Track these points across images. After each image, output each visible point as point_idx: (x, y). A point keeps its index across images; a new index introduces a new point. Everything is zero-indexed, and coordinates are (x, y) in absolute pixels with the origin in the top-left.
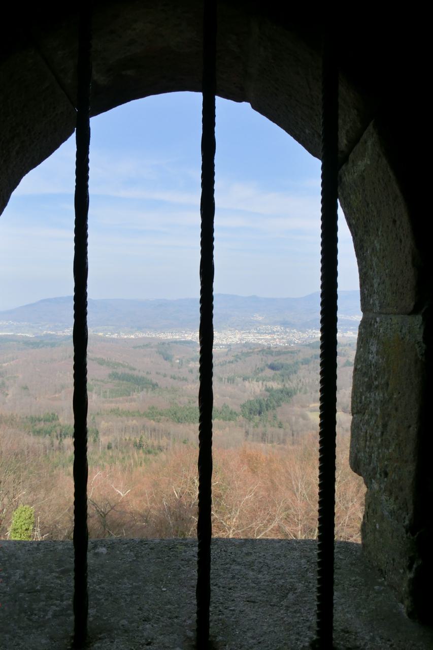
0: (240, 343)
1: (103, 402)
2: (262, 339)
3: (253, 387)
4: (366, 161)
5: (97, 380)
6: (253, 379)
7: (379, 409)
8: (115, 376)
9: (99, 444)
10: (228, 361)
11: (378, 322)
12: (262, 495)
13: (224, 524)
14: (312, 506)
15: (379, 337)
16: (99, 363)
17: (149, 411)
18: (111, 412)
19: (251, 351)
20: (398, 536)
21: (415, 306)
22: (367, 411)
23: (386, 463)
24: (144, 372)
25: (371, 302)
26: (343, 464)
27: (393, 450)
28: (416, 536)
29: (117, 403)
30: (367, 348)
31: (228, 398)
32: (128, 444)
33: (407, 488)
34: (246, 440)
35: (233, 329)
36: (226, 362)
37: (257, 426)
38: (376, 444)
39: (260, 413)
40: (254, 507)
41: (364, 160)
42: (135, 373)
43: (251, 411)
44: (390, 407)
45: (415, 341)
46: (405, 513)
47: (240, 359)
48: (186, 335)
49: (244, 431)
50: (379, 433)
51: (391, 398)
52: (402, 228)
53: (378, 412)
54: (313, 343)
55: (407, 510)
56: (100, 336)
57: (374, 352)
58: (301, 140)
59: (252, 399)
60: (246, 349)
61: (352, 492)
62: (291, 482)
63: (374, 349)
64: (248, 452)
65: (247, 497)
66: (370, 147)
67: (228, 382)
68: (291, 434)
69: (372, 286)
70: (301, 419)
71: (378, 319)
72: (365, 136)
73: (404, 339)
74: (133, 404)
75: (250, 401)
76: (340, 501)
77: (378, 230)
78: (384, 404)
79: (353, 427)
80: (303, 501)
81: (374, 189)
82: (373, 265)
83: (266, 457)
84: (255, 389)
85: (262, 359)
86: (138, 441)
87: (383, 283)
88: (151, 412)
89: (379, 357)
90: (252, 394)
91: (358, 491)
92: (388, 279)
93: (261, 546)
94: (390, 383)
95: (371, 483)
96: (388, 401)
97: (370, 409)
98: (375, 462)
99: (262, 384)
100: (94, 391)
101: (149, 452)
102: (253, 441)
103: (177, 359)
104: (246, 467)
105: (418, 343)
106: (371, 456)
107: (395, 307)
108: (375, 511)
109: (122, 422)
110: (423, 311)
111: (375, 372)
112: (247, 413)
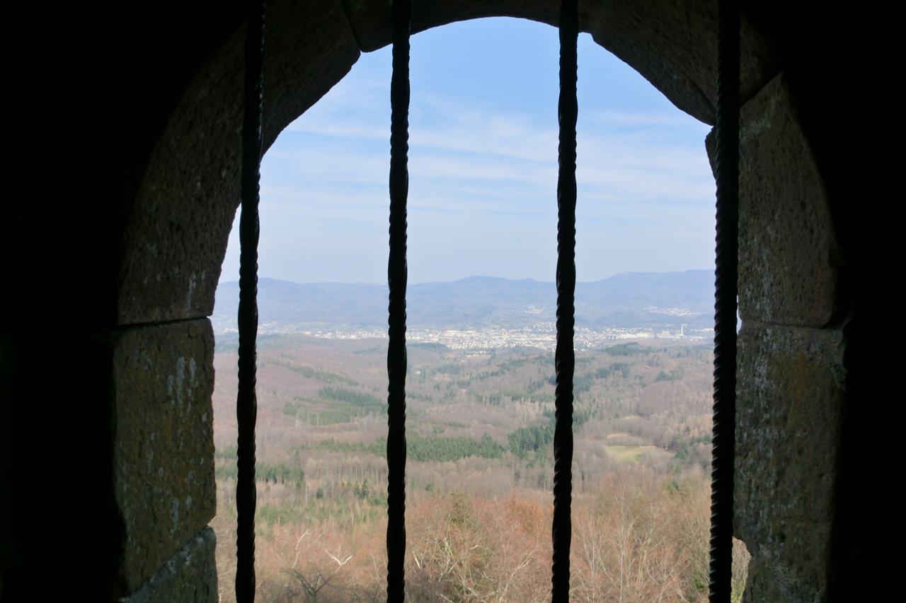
0: (509, 347)
2: (539, 341)
4: (764, 121)
5: (303, 399)
6: (526, 398)
7: (772, 452)
8: (327, 393)
10: (490, 373)
11: (770, 335)
12: (540, 564)
14: (611, 579)
15: (770, 356)
16: (305, 375)
17: (376, 443)
18: (322, 444)
19: (524, 358)
22: (750, 453)
23: (783, 522)
25: (758, 307)
26: (656, 521)
27: (795, 506)
31: (490, 425)
32: (346, 492)
33: (817, 557)
34: (515, 485)
36: (488, 373)
37: (531, 465)
38: (766, 498)
39: (536, 447)
40: (530, 580)
41: (761, 121)
42: (358, 389)
44: (789, 449)
47: (508, 370)
48: (430, 335)
49: (513, 473)
50: (772, 483)
51: (791, 437)
53: (771, 454)
54: (613, 347)
55: (817, 584)
56: (307, 336)
57: (762, 374)
59: (525, 426)
60: (516, 356)
62: (582, 546)
63: (763, 370)
64: (518, 502)
65: (519, 567)
66: (773, 107)
67: (491, 402)
68: (581, 478)
69: (759, 285)
70: (594, 457)
71: (769, 331)
72: (766, 90)
73: (814, 360)
74: (354, 433)
77: (773, 213)
78: (779, 446)
79: (204, 418)
81: (774, 160)
82: (762, 258)
84: (529, 413)
85: (539, 370)
86: (361, 487)
87: (780, 283)
88: (380, 445)
89: (772, 382)
90: (525, 420)
91: (676, 559)
92: (787, 278)
94: (789, 417)
96: (787, 441)
97: (756, 451)
99: (540, 405)
100: (298, 414)
101: (377, 502)
102: (525, 486)
103: (418, 369)
104: (517, 525)
105: (835, 366)
106: (758, 513)
108: (764, 586)
110: (844, 325)
111: (765, 403)
112: (518, 447)
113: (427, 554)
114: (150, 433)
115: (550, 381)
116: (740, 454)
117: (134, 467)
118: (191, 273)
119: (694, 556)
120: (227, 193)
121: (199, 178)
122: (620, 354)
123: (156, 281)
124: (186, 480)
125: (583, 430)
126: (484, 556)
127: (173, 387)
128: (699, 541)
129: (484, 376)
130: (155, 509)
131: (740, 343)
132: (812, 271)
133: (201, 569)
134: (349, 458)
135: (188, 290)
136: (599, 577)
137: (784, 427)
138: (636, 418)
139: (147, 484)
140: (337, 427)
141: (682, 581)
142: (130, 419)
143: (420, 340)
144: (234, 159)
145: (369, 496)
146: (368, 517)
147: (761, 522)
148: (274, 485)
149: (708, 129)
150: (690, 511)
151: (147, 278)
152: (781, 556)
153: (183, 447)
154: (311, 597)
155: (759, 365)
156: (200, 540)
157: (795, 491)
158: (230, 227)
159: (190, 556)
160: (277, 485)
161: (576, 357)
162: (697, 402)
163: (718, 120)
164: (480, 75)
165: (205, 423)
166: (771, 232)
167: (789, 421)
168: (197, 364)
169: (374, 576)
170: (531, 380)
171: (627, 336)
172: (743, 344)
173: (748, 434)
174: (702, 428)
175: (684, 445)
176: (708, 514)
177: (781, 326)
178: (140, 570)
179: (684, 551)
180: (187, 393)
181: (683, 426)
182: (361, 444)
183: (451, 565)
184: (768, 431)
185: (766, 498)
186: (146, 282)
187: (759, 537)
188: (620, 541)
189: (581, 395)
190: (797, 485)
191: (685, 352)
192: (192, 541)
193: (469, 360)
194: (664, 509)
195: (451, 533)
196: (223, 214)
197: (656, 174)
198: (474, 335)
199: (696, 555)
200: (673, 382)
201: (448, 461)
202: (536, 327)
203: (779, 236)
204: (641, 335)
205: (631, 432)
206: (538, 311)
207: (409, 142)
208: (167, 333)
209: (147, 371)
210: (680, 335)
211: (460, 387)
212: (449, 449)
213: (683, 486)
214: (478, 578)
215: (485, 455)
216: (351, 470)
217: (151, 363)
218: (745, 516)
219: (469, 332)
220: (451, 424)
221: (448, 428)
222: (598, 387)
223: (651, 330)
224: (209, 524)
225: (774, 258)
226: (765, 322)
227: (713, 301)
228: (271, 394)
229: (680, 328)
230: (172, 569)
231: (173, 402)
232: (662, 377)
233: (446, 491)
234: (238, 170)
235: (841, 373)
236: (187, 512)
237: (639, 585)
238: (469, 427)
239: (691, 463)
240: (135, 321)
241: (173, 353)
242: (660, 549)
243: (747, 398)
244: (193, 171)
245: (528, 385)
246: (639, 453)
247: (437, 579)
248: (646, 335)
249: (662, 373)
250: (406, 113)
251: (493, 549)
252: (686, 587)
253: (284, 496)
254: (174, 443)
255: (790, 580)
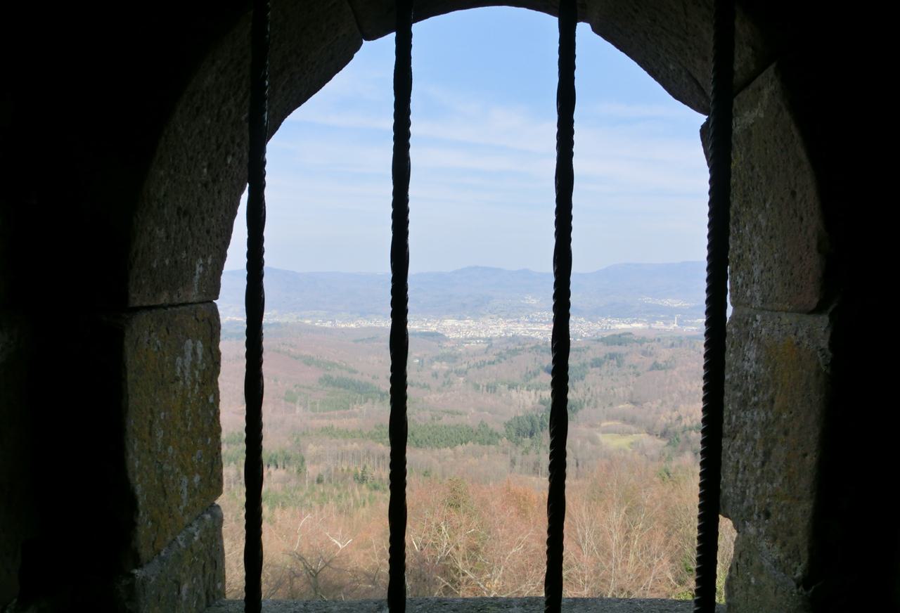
0: (506, 337)
1: (312, 418)
2: (536, 331)
3: (522, 398)
4: (758, 110)
7: (759, 433)
8: (328, 381)
9: (305, 475)
10: (487, 361)
13: (482, 586)
14: (603, 563)
15: (759, 340)
19: (521, 347)
20: (784, 592)
21: (819, 304)
22: (738, 435)
23: (768, 500)
24: (368, 375)
25: (748, 293)
27: (780, 485)
28: (811, 591)
29: (330, 419)
30: (741, 354)
31: (487, 413)
32: (345, 478)
33: (800, 532)
35: (495, 316)
37: (526, 452)
39: (531, 435)
40: (523, 563)
41: (754, 111)
42: (357, 377)
43: (519, 432)
44: (775, 430)
45: (817, 348)
46: (796, 563)
47: (505, 359)
48: (429, 324)
49: (509, 459)
50: (759, 463)
51: (778, 419)
52: (805, 202)
53: (758, 436)
55: (800, 558)
57: (751, 359)
58: (660, 76)
59: (520, 414)
61: (659, 544)
62: (575, 531)
63: (752, 355)
65: (514, 550)
66: (766, 97)
67: (488, 391)
68: (575, 464)
69: (750, 273)
70: (588, 444)
71: (758, 317)
72: (759, 80)
73: (801, 345)
74: (353, 420)
75: (518, 419)
76: (642, 556)
77: (765, 202)
79: (211, 400)
80: (591, 555)
81: (766, 149)
82: (753, 246)
83: (539, 497)
84: (524, 401)
85: (535, 359)
86: (360, 472)
87: (769, 270)
88: (379, 431)
89: (761, 366)
90: (521, 407)
91: (667, 543)
93: (596, 606)
95: (744, 525)
96: (774, 422)
98: (751, 500)
99: (536, 393)
101: (376, 488)
103: (416, 358)
104: (513, 509)
105: (821, 350)
106: (744, 492)
107: (788, 303)
109: (338, 446)
110: (830, 310)
111: (754, 386)
113: (424, 538)
114: (159, 412)
115: (546, 370)
116: (729, 436)
117: (145, 444)
118: (198, 258)
119: (684, 541)
120: (232, 179)
121: (205, 164)
122: (615, 344)
123: (164, 264)
124: (194, 459)
125: (578, 417)
126: (480, 540)
127: (181, 368)
128: (689, 525)
129: (481, 366)
130: (165, 486)
131: (730, 329)
132: (801, 258)
133: (208, 543)
134: (349, 445)
135: (195, 274)
136: (592, 559)
137: (771, 409)
138: (631, 406)
139: (157, 462)
140: (336, 414)
141: (671, 565)
142: (141, 398)
143: (419, 329)
144: (239, 145)
145: (369, 481)
146: (367, 501)
147: (748, 501)
148: (275, 470)
149: (702, 119)
150: (680, 497)
151: (155, 262)
152: (765, 532)
153: (191, 426)
154: (312, 579)
155: (748, 350)
156: (208, 517)
157: (780, 470)
158: (234, 214)
159: (199, 531)
160: (278, 470)
161: (572, 346)
162: (690, 391)
163: (712, 109)
164: (482, 68)
165: (212, 404)
166: (762, 221)
167: (776, 404)
168: (204, 347)
169: (374, 557)
170: (527, 368)
171: (621, 326)
172: (733, 330)
173: (737, 417)
174: (694, 417)
175: (675, 433)
176: (696, 501)
177: (770, 312)
178: (151, 544)
179: (674, 535)
180: (195, 374)
181: (675, 415)
182: (360, 431)
183: (447, 549)
184: (755, 413)
185: (753, 478)
186: (155, 266)
187: (745, 514)
188: (612, 526)
189: (576, 384)
190: (783, 469)
191: (678, 342)
192: (199, 518)
193: (466, 348)
194: (656, 495)
195: (449, 517)
196: (229, 200)
197: (651, 162)
198: (471, 325)
199: (686, 540)
200: (666, 372)
201: (445, 447)
202: (533, 317)
203: (770, 224)
204: (635, 325)
205: (624, 420)
206: (535, 301)
207: (411, 129)
208: (176, 316)
209: (156, 352)
210: (674, 326)
211: (457, 376)
212: (447, 436)
213: (675, 473)
214: (474, 560)
215: (481, 443)
216: (351, 456)
217: (160, 345)
218: (733, 495)
219: (466, 321)
220: (448, 412)
221: (446, 416)
222: (592, 376)
223: (645, 320)
224: (217, 502)
225: (765, 245)
226: (755, 308)
227: (704, 296)
228: (273, 381)
229: (674, 319)
230: (181, 543)
231: (181, 383)
232: (656, 366)
233: (444, 476)
234: (243, 156)
235: (827, 356)
236: (195, 490)
237: (630, 568)
238: (466, 414)
239: (682, 451)
240: (145, 304)
241: (181, 335)
242: (651, 532)
243: (736, 382)
244: (200, 156)
245: (524, 373)
246: (632, 441)
247: (434, 562)
248: (640, 326)
249: (655, 363)
250: (409, 101)
251: (489, 533)
252: (676, 571)
253: (285, 481)
254: (182, 423)
255: (773, 555)
